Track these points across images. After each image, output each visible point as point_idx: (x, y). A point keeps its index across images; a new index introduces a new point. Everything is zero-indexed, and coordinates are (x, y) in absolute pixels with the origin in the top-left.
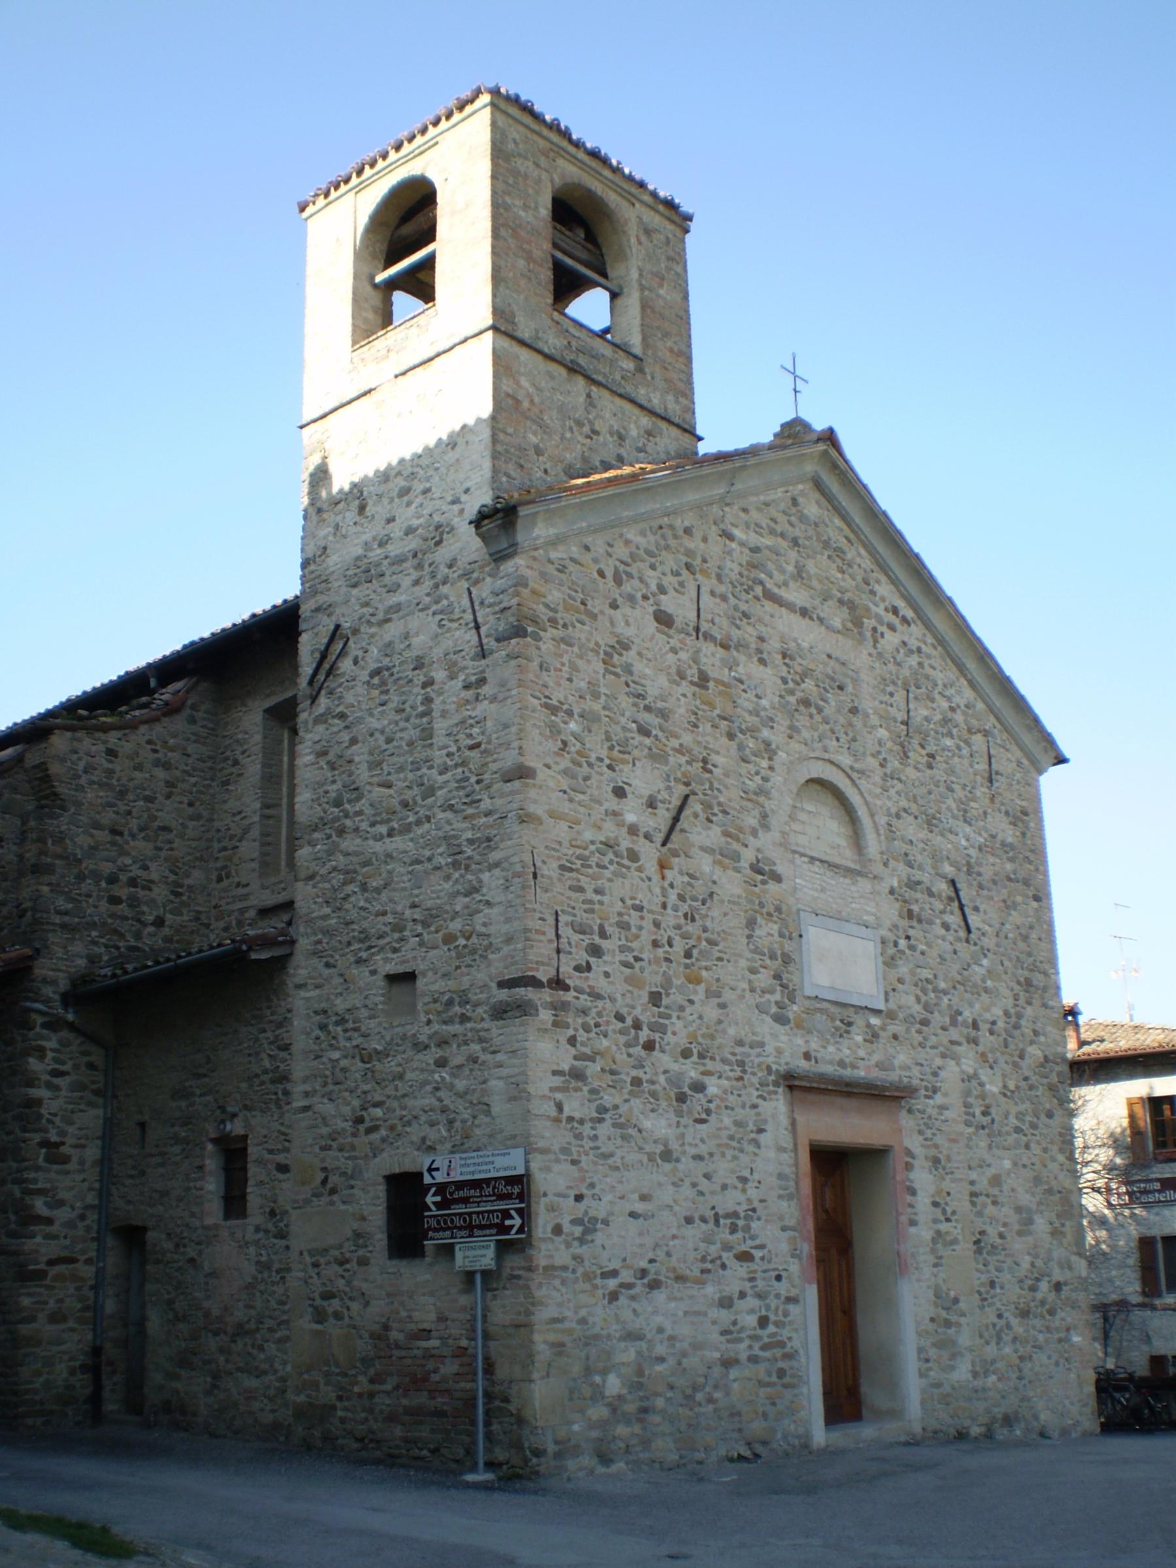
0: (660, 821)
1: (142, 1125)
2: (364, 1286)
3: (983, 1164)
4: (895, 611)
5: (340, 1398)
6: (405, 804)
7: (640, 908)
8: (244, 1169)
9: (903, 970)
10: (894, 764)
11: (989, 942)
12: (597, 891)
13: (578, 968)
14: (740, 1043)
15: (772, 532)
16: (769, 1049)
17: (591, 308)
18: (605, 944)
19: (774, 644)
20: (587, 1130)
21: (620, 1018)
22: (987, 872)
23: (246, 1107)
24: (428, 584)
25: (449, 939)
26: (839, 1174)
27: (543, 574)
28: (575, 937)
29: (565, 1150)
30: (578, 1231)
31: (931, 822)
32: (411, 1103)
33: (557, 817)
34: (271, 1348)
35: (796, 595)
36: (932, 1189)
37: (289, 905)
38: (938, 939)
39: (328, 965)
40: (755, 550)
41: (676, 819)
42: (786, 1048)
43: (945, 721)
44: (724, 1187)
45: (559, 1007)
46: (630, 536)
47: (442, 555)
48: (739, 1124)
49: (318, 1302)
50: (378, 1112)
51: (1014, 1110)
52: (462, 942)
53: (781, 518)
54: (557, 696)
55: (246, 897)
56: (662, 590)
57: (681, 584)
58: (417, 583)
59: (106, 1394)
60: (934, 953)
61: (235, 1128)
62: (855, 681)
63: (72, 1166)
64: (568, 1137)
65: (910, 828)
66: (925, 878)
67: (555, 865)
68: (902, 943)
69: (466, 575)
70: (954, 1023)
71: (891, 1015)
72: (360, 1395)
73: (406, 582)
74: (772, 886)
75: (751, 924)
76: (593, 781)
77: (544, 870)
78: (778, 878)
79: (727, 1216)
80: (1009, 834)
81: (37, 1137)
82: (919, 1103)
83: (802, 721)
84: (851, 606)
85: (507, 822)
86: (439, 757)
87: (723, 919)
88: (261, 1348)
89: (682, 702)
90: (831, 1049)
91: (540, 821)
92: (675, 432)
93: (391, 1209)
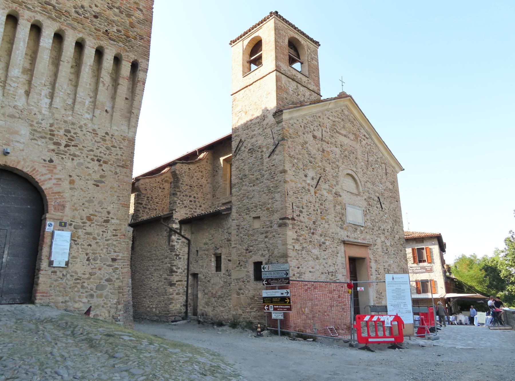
0: (315, 182)
1: (197, 251)
2: (249, 287)
3: (386, 262)
4: (365, 136)
5: (243, 313)
6: (257, 179)
7: (310, 202)
8: (221, 261)
9: (368, 217)
10: (365, 170)
11: (387, 211)
12: (301, 198)
13: (297, 216)
14: (333, 233)
15: (338, 117)
16: (339, 235)
17: (297, 66)
18: (303, 210)
19: (339, 143)
20: (300, 252)
21: (307, 227)
22: (386, 195)
23: (221, 247)
24: (261, 129)
25: (268, 209)
26: (355, 264)
27: (288, 126)
28: (297, 208)
29: (295, 257)
30: (298, 275)
31: (373, 184)
32: (259, 246)
33: (293, 181)
34: (227, 301)
35: (343, 132)
36: (375, 267)
37: (230, 202)
38: (375, 210)
39: (239, 215)
40: (334, 122)
41: (318, 182)
42: (343, 235)
43: (376, 161)
44: (330, 266)
45: (293, 224)
46: (307, 118)
47: (265, 122)
48: (333, 251)
49: (238, 291)
50: (252, 248)
51: (393, 249)
52: (271, 209)
53: (340, 114)
54: (292, 154)
55: (219, 201)
56: (314, 130)
57: (318, 129)
58: (259, 129)
59: (189, 311)
60: (374, 213)
61: (219, 251)
62: (357, 152)
63: (182, 260)
64: (296, 254)
65: (369, 185)
66: (372, 196)
67: (292, 192)
68: (368, 211)
69: (270, 127)
70: (379, 229)
71: (365, 227)
72: (248, 312)
73: (256, 129)
74: (339, 198)
75: (335, 206)
76: (300, 173)
77: (289, 193)
78: (340, 196)
79: (331, 272)
80: (391, 187)
81: (174, 253)
82: (372, 248)
83: (345, 161)
84: (355, 134)
85: (281, 183)
86: (265, 168)
87: (329, 205)
88: (225, 301)
89: (319, 156)
90: (353, 235)
91: (289, 182)
92: (316, 95)
93: (254, 270)
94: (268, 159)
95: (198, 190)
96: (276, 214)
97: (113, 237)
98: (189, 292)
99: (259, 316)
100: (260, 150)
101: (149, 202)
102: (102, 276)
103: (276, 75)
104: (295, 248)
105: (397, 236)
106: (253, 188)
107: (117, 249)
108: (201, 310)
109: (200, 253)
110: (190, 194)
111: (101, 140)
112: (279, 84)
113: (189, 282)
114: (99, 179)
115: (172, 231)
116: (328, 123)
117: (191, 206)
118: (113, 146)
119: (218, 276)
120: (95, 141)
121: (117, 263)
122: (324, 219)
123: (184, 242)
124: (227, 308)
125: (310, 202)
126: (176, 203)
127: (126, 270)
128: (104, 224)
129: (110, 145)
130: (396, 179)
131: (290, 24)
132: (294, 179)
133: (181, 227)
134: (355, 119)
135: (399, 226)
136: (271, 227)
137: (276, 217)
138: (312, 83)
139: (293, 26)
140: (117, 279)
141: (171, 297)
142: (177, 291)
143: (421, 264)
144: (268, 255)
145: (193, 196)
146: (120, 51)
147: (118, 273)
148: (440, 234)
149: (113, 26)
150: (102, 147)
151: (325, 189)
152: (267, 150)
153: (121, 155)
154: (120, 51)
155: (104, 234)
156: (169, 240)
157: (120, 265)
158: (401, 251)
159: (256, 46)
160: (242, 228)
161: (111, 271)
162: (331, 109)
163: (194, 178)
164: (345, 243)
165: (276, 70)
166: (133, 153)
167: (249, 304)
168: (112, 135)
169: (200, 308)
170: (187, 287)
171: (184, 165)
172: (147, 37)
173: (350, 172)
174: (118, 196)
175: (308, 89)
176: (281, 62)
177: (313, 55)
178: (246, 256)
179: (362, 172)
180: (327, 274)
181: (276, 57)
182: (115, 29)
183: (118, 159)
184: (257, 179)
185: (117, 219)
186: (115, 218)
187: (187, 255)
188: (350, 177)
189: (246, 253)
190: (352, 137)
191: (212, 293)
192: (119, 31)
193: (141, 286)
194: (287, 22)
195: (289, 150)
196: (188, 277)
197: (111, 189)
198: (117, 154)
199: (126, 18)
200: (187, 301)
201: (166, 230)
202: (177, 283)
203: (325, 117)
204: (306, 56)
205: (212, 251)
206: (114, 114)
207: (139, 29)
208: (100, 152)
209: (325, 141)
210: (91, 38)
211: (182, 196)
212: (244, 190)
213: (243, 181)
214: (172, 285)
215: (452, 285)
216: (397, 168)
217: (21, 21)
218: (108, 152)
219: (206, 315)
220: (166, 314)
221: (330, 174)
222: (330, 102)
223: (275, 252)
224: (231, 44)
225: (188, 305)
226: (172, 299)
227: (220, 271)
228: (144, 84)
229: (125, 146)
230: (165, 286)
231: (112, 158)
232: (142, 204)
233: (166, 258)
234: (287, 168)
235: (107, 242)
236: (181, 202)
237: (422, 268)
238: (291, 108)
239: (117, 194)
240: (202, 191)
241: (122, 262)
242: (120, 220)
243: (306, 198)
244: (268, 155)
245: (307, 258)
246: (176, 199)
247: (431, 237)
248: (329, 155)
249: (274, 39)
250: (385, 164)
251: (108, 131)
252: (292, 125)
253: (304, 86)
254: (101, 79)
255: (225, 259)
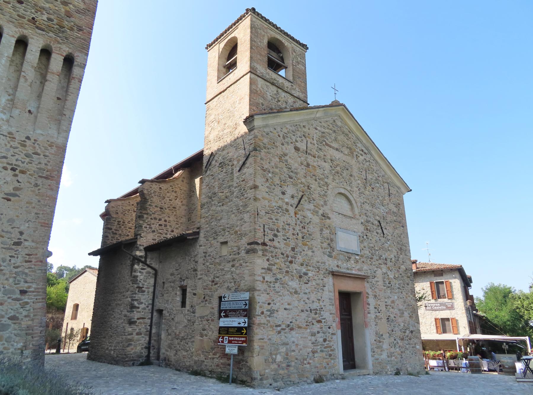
1: (164, 283)
4: (362, 151)
5: (205, 359)
7: (289, 225)
9: (366, 244)
12: (276, 220)
13: (270, 240)
14: (318, 262)
15: (328, 128)
16: (327, 264)
18: (278, 234)
20: (272, 285)
21: (282, 254)
23: (187, 278)
25: (236, 232)
26: (347, 301)
27: (262, 135)
28: (269, 232)
29: (265, 290)
30: (269, 313)
31: (373, 205)
32: (225, 276)
34: (190, 344)
38: (375, 237)
39: (207, 240)
40: (323, 133)
41: (300, 201)
42: (332, 264)
43: (376, 179)
44: (313, 302)
45: (264, 251)
46: (288, 127)
48: (318, 284)
50: (217, 279)
51: (397, 283)
52: (239, 233)
53: (331, 125)
54: (266, 167)
56: (296, 141)
59: (151, 355)
60: (374, 240)
61: (184, 283)
62: (352, 168)
64: (266, 286)
65: (367, 207)
66: (371, 220)
67: (264, 212)
70: (380, 259)
71: (362, 256)
72: (210, 358)
74: (328, 220)
75: (321, 230)
78: (329, 218)
79: (314, 310)
80: (395, 210)
81: (136, 286)
84: (350, 149)
87: (314, 229)
88: (187, 344)
89: (301, 171)
90: (345, 264)
92: (301, 102)
94: (238, 174)
95: (170, 212)
96: (244, 238)
97: (25, 264)
98: (154, 331)
99: (222, 364)
100: (231, 164)
101: (120, 227)
102: (3, 313)
103: (250, 78)
104: (266, 280)
105: (402, 267)
106: (222, 208)
107: (29, 279)
108: (164, 353)
109: (166, 286)
110: (160, 217)
111: (19, 146)
112: (254, 87)
113: (154, 319)
114: (12, 191)
115: (137, 260)
116: (316, 135)
117: (161, 231)
118: (36, 154)
119: (182, 312)
120: (11, 146)
121: (27, 297)
122: (306, 245)
123: (150, 273)
124: (189, 352)
125: (287, 224)
126: (142, 227)
127: (39, 305)
128: (14, 247)
129: (30, 152)
130: (402, 201)
131: (270, 23)
132: (267, 196)
133: (146, 254)
134: (351, 131)
135: (406, 255)
136: (239, 253)
137: (244, 241)
138: (297, 89)
139: (274, 26)
140: (25, 316)
141: (129, 337)
142: (138, 330)
143: (440, 300)
144: (234, 288)
145: (163, 220)
146: (50, 42)
147: (27, 309)
148: (461, 266)
149: (42, 14)
150: (20, 153)
151: (310, 210)
152: (238, 163)
153: (46, 164)
154: (50, 42)
155: (13, 259)
156: (132, 270)
157: (32, 299)
158: (408, 284)
159: (232, 50)
160: (209, 256)
161: (18, 306)
162: (319, 118)
163: (166, 198)
164: (334, 274)
165: (250, 72)
166: (62, 162)
167: (213, 349)
168: (35, 140)
169: (163, 351)
170: (151, 326)
171: (154, 184)
172: (87, 29)
173: (343, 191)
174: (36, 214)
175: (292, 95)
176: (258, 63)
177: (299, 59)
178: (211, 289)
179: (358, 192)
180: (309, 312)
181: (251, 58)
182: (45, 17)
183: (40, 169)
184: (226, 197)
185: (33, 241)
186: (30, 240)
187: (153, 288)
188: (343, 197)
189: (212, 285)
190: (346, 151)
191: (175, 334)
192: (49, 19)
193: (102, 323)
194: (266, 20)
195: (262, 162)
196: (152, 313)
197: (28, 205)
198: (40, 163)
199: (61, 6)
200: (149, 342)
201: (130, 258)
202: (138, 321)
203: (311, 128)
204: (291, 59)
205: (178, 283)
206: (39, 115)
207: (77, 19)
208: (17, 160)
209: (311, 155)
210: (11, 25)
211: (149, 219)
212: (213, 210)
213: (213, 201)
214: (131, 323)
215: (479, 323)
216: (403, 189)
217: (54, 56)
218: (27, 160)
219: (169, 361)
220: (123, 358)
221: (317, 192)
222: (317, 110)
223: (242, 285)
224: (207, 48)
225: (152, 348)
226: (131, 340)
227: (185, 307)
228: (80, 81)
229: (52, 154)
230: (124, 325)
231: (33, 167)
232: (111, 229)
233: (128, 292)
234: (257, 184)
235: (16, 270)
236: (148, 226)
237: (441, 304)
238: (266, 114)
239: (35, 211)
240: (175, 213)
241: (35, 296)
242: (37, 243)
243: (282, 219)
244: (238, 169)
245: (282, 292)
246: (141, 222)
247: (451, 270)
248: (316, 170)
249: (249, 38)
250: (388, 183)
251: (30, 136)
252: (268, 134)
253: (286, 92)
254: (23, 74)
255: (190, 292)
